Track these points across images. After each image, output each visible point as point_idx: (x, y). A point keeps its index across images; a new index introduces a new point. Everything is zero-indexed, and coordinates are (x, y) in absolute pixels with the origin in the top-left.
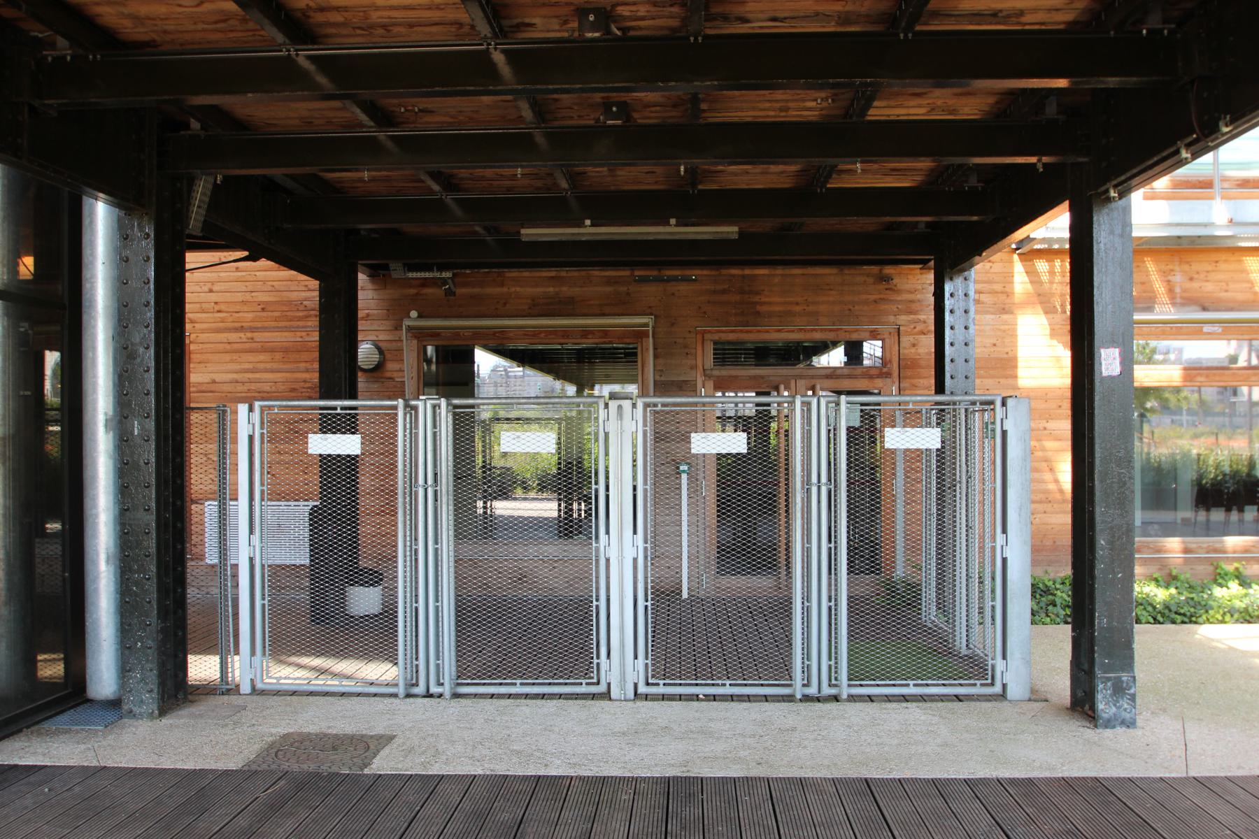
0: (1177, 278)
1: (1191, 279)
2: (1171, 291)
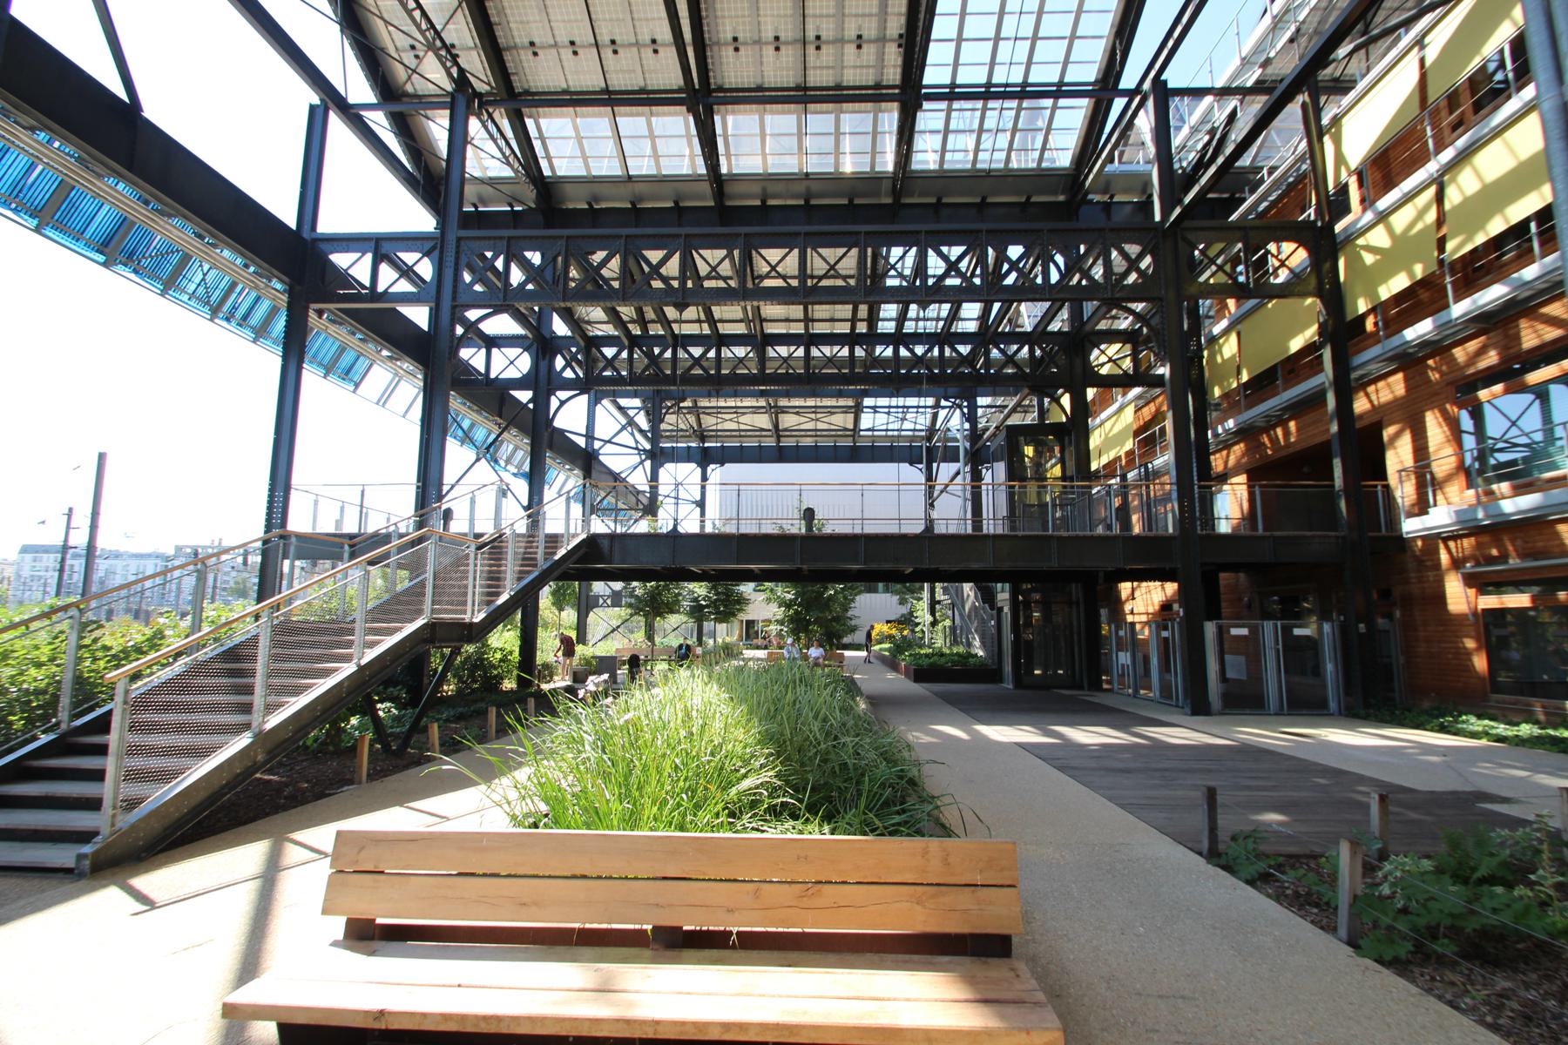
0: (1519, 542)
1: (1527, 542)
2: (1516, 550)
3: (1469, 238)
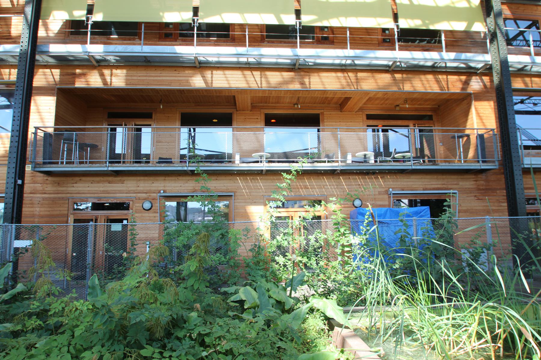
3: (320, 20)
